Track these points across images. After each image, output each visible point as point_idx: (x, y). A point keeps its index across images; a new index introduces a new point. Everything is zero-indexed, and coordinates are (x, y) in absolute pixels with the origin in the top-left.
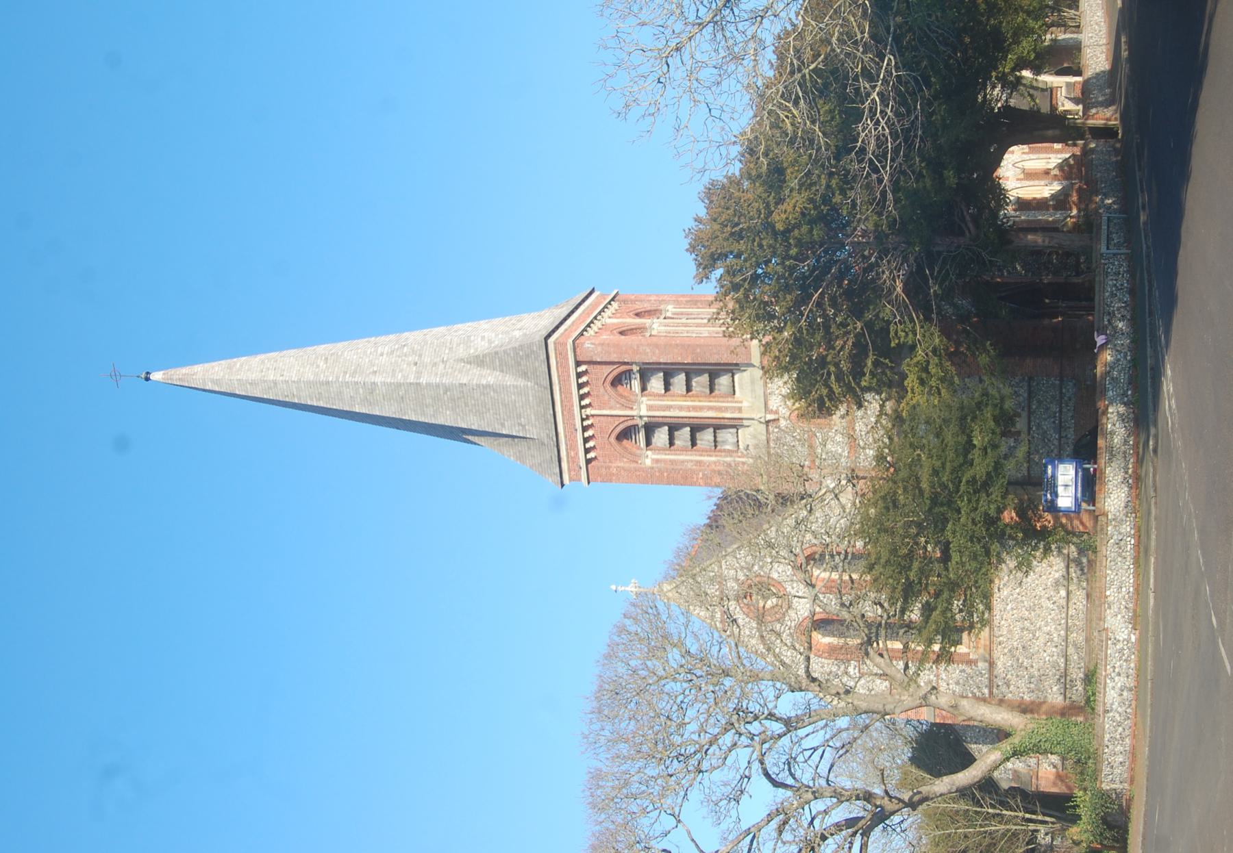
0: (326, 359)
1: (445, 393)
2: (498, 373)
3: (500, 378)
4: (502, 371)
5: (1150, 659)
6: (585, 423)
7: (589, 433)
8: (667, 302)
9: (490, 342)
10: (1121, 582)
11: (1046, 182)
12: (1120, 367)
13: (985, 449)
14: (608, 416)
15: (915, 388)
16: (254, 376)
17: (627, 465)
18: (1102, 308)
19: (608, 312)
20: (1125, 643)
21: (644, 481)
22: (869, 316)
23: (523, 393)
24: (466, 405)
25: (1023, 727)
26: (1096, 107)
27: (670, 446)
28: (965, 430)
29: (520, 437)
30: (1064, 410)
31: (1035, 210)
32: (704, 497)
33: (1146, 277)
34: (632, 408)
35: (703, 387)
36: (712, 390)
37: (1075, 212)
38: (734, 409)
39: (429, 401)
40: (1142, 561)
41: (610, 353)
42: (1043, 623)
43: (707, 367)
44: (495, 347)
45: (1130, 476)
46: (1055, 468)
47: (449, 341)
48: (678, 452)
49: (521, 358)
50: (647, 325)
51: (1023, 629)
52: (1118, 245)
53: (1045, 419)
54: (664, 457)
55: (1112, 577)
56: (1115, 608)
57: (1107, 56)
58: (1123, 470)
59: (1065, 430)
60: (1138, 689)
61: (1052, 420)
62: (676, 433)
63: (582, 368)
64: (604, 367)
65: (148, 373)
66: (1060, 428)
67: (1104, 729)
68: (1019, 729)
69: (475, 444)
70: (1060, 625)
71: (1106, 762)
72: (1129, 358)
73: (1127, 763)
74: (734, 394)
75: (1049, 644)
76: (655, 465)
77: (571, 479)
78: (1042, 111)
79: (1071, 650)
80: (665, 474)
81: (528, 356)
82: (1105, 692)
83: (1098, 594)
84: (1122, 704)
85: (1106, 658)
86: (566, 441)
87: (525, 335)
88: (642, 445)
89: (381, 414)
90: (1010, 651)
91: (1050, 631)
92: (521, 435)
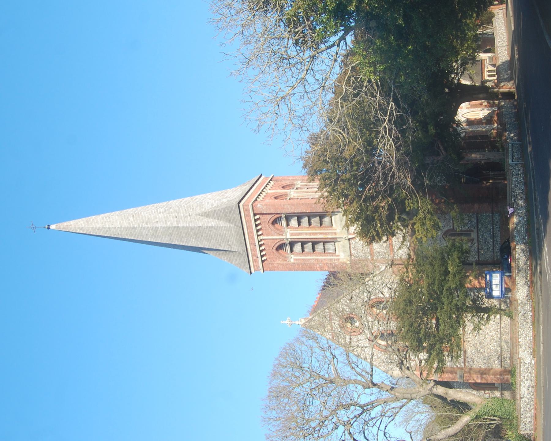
0: (133, 216)
2: (216, 220)
3: (217, 223)
4: (218, 219)
5: (542, 377)
6: (260, 243)
9: (212, 205)
10: (526, 335)
12: (521, 225)
14: (271, 239)
16: (99, 225)
17: (282, 262)
19: (269, 187)
20: (529, 364)
21: (291, 270)
22: (394, 196)
23: (229, 229)
24: (202, 236)
25: (480, 403)
26: (504, 82)
27: (302, 252)
28: (444, 263)
29: (229, 251)
30: (495, 228)
31: (476, 125)
32: (317, 293)
35: (317, 223)
36: (321, 224)
38: (332, 234)
39: (184, 235)
40: (536, 324)
41: (270, 209)
42: (489, 331)
44: (215, 207)
45: (529, 281)
46: (491, 276)
47: (192, 205)
48: (306, 255)
49: (227, 213)
50: (288, 193)
52: (518, 159)
53: (485, 233)
55: (521, 332)
56: (523, 347)
57: (508, 52)
58: (524, 278)
59: (496, 237)
60: (537, 387)
61: (489, 233)
62: (305, 246)
63: (257, 217)
64: (268, 215)
65: (49, 226)
66: (493, 237)
67: (520, 407)
68: (478, 404)
69: (206, 253)
70: (497, 332)
71: (522, 422)
72: (525, 219)
73: (533, 422)
74: (332, 226)
75: (492, 341)
76: (296, 262)
77: (255, 270)
79: (503, 344)
80: (301, 266)
81: (230, 212)
82: (520, 389)
83: (515, 341)
84: (529, 394)
85: (520, 372)
86: (251, 252)
87: (229, 201)
88: (289, 252)
89: (161, 242)
90: (473, 345)
91: (493, 335)
92: (230, 250)
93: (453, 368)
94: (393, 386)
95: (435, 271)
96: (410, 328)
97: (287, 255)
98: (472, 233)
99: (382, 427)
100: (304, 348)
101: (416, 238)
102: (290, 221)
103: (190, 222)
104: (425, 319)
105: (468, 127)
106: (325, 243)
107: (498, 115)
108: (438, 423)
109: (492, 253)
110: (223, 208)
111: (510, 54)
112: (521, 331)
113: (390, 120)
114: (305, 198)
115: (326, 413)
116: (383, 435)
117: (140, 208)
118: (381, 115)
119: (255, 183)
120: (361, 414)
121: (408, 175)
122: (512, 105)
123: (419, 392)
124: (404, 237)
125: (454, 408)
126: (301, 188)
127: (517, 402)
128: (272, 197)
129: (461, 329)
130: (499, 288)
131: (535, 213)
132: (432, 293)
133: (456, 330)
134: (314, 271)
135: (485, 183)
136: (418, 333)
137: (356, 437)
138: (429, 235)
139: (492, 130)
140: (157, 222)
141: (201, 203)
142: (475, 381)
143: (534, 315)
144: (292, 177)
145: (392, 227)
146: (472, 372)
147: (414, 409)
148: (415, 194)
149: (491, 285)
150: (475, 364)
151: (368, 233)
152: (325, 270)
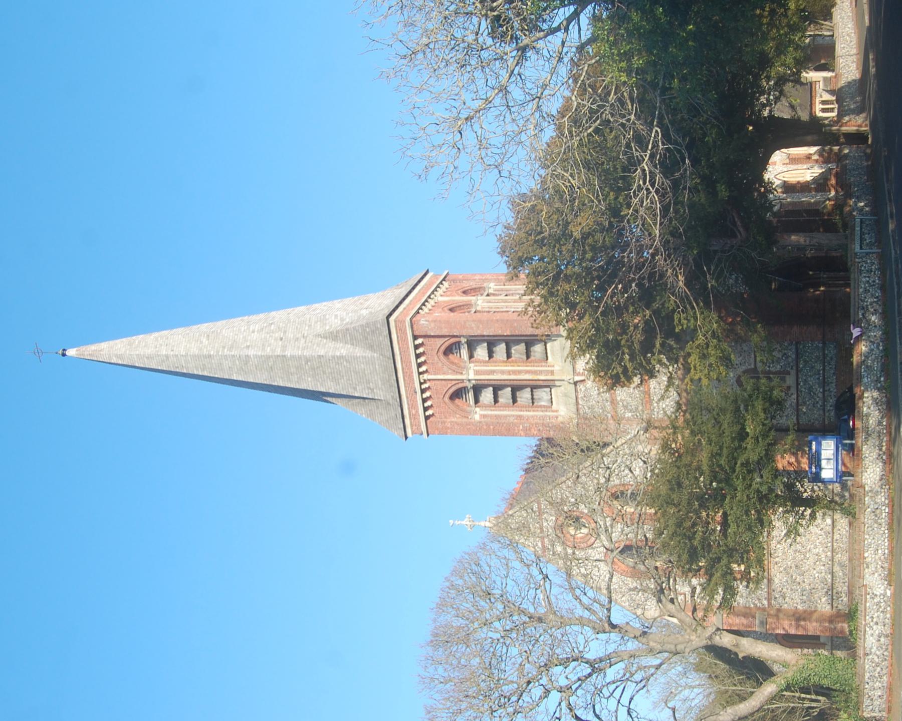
0: (208, 336)
1: (306, 363)
2: (349, 346)
3: (351, 350)
4: (353, 345)
6: (423, 386)
7: (427, 394)
8: (489, 281)
9: (342, 320)
11: (809, 166)
12: (873, 356)
13: (757, 439)
15: (697, 365)
17: (459, 420)
18: (857, 304)
19: (440, 291)
20: (882, 597)
22: (656, 306)
24: (324, 372)
26: (849, 114)
30: (827, 368)
31: (798, 192)
33: (895, 280)
34: (462, 373)
35: (521, 354)
36: (528, 357)
37: (833, 193)
38: (547, 373)
39: (293, 370)
43: (523, 338)
44: (347, 324)
45: (884, 453)
46: (819, 445)
51: (795, 551)
52: (870, 245)
53: (811, 376)
54: (490, 413)
55: (870, 541)
56: (872, 568)
57: (857, 65)
59: (828, 385)
61: (817, 377)
62: (500, 392)
64: (437, 339)
65: (64, 350)
66: (824, 383)
69: (331, 403)
72: (881, 348)
74: (547, 359)
75: (818, 563)
78: (802, 119)
79: (837, 568)
80: (492, 427)
82: (865, 638)
85: (865, 610)
86: (408, 401)
87: (371, 313)
88: (471, 403)
90: (785, 569)
92: (371, 397)
93: (749, 608)
94: (646, 630)
95: (724, 433)
96: (678, 530)
97: (469, 409)
98: (787, 377)
99: (625, 700)
100: (494, 562)
101: (692, 380)
102: (475, 349)
103: (303, 349)
104: (704, 514)
105: (785, 195)
106: (533, 388)
107: (837, 175)
108: (720, 704)
109: (821, 412)
110: (362, 326)
111: (861, 68)
112: (868, 539)
113: (652, 156)
114: (502, 312)
115: (530, 669)
116: (626, 713)
117: (220, 323)
118: (636, 150)
119: (416, 285)
120: (590, 675)
121: (680, 269)
122: (862, 154)
123: (690, 641)
124: (670, 378)
125: (748, 678)
126: (494, 295)
127: (860, 662)
128: (445, 309)
129: (765, 534)
130: (832, 464)
131: (898, 336)
132: (717, 469)
133: (755, 536)
134: (513, 435)
135: (812, 291)
136: (691, 539)
137: (580, 713)
138: (714, 375)
139: (825, 201)
140: (248, 347)
141: (324, 316)
142: (787, 631)
143: (893, 512)
144: (481, 275)
145: (650, 360)
146: (781, 615)
147: (679, 680)
148: (690, 303)
149: (819, 460)
150: (786, 603)
151: (609, 370)
152: (533, 436)
